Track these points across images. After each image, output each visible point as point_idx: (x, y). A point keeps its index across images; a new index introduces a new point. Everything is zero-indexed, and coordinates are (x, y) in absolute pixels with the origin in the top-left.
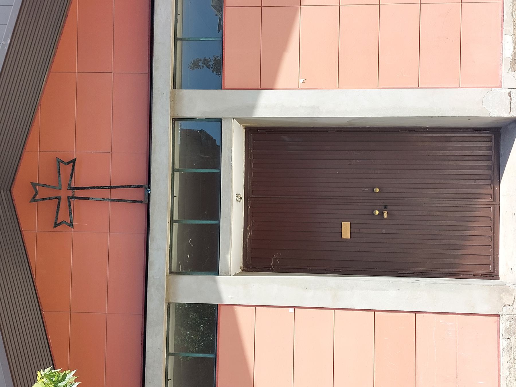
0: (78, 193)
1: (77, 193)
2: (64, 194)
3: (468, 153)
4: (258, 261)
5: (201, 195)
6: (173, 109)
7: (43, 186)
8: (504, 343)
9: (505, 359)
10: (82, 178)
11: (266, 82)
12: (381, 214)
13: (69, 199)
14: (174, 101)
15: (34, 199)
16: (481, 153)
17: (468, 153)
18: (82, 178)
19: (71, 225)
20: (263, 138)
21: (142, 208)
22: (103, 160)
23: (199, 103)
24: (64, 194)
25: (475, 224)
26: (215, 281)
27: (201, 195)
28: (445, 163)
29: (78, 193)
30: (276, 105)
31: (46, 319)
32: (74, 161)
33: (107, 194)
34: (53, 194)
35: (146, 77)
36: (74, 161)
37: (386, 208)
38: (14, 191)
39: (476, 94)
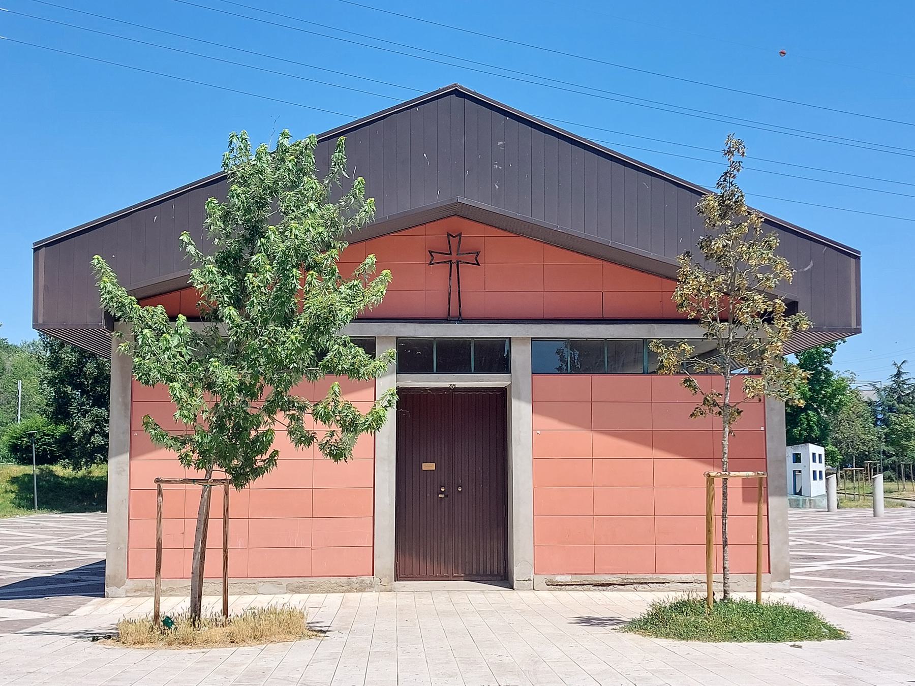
0: (454, 266)
1: (454, 266)
2: (454, 257)
3: (488, 557)
4: (407, 400)
5: (453, 356)
6: (517, 338)
7: (459, 242)
8: (354, 579)
9: (346, 579)
10: (465, 269)
11: (537, 407)
12: (442, 493)
13: (450, 254)
14: (523, 339)
15: (449, 235)
16: (488, 566)
17: (488, 557)
18: (467, 271)
19: (431, 263)
20: (499, 400)
21: (442, 314)
22: (481, 287)
23: (521, 357)
24: (454, 257)
25: (435, 563)
26: (392, 373)
27: (453, 356)
28: (481, 540)
29: (454, 266)
30: (521, 413)
31: (360, 244)
32: (478, 264)
33: (454, 287)
34: (454, 248)
35: (539, 315)
36: (478, 264)
37: (447, 496)
38: (455, 217)
39: (530, 556)
